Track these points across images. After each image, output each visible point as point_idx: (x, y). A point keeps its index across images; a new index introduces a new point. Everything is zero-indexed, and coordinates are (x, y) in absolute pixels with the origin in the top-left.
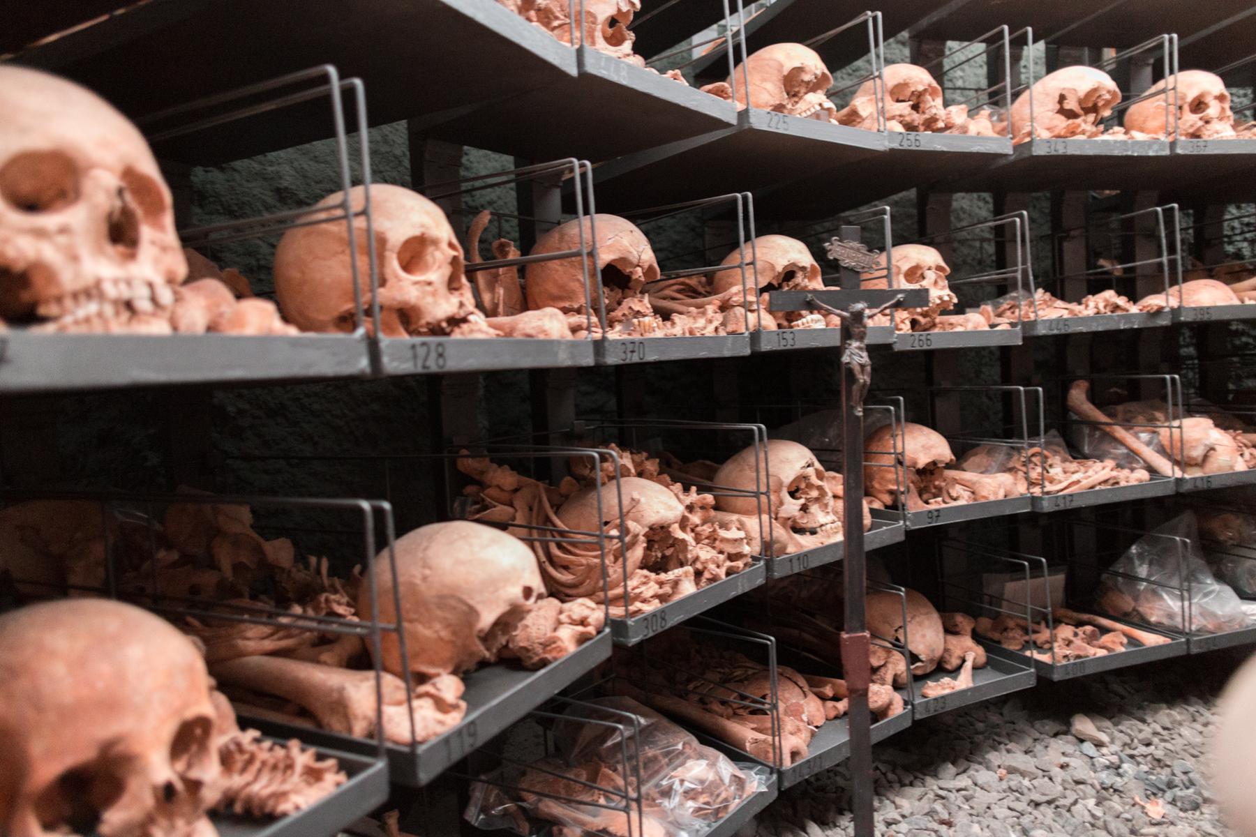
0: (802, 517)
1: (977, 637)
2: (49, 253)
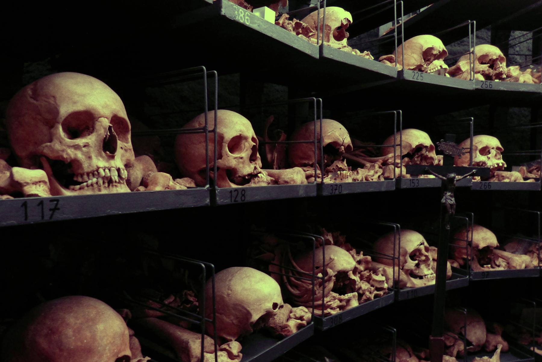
0: (416, 270)
1: (505, 337)
2: (80, 155)
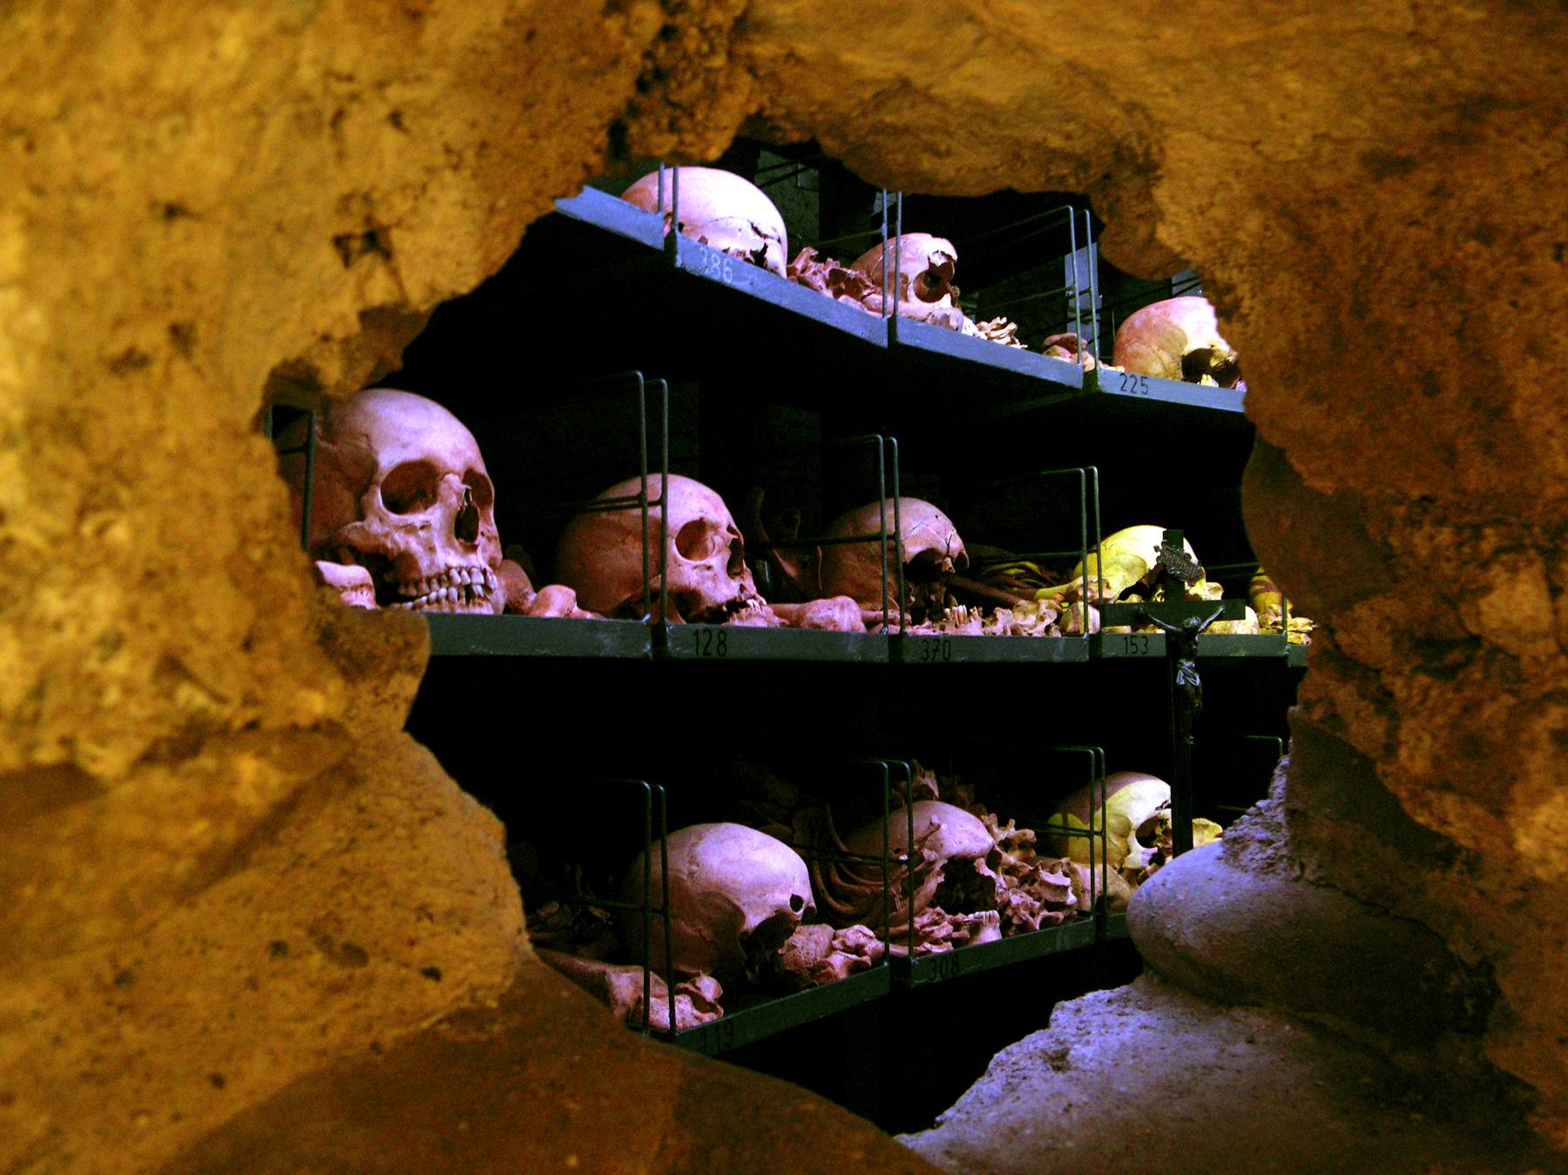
2: (414, 546)
